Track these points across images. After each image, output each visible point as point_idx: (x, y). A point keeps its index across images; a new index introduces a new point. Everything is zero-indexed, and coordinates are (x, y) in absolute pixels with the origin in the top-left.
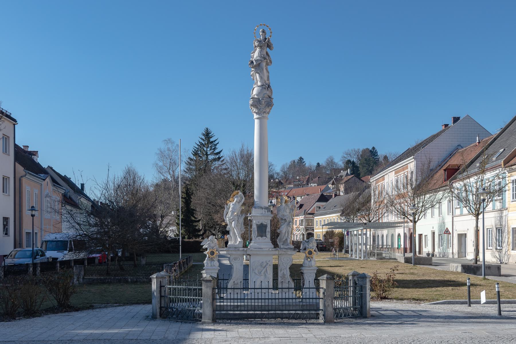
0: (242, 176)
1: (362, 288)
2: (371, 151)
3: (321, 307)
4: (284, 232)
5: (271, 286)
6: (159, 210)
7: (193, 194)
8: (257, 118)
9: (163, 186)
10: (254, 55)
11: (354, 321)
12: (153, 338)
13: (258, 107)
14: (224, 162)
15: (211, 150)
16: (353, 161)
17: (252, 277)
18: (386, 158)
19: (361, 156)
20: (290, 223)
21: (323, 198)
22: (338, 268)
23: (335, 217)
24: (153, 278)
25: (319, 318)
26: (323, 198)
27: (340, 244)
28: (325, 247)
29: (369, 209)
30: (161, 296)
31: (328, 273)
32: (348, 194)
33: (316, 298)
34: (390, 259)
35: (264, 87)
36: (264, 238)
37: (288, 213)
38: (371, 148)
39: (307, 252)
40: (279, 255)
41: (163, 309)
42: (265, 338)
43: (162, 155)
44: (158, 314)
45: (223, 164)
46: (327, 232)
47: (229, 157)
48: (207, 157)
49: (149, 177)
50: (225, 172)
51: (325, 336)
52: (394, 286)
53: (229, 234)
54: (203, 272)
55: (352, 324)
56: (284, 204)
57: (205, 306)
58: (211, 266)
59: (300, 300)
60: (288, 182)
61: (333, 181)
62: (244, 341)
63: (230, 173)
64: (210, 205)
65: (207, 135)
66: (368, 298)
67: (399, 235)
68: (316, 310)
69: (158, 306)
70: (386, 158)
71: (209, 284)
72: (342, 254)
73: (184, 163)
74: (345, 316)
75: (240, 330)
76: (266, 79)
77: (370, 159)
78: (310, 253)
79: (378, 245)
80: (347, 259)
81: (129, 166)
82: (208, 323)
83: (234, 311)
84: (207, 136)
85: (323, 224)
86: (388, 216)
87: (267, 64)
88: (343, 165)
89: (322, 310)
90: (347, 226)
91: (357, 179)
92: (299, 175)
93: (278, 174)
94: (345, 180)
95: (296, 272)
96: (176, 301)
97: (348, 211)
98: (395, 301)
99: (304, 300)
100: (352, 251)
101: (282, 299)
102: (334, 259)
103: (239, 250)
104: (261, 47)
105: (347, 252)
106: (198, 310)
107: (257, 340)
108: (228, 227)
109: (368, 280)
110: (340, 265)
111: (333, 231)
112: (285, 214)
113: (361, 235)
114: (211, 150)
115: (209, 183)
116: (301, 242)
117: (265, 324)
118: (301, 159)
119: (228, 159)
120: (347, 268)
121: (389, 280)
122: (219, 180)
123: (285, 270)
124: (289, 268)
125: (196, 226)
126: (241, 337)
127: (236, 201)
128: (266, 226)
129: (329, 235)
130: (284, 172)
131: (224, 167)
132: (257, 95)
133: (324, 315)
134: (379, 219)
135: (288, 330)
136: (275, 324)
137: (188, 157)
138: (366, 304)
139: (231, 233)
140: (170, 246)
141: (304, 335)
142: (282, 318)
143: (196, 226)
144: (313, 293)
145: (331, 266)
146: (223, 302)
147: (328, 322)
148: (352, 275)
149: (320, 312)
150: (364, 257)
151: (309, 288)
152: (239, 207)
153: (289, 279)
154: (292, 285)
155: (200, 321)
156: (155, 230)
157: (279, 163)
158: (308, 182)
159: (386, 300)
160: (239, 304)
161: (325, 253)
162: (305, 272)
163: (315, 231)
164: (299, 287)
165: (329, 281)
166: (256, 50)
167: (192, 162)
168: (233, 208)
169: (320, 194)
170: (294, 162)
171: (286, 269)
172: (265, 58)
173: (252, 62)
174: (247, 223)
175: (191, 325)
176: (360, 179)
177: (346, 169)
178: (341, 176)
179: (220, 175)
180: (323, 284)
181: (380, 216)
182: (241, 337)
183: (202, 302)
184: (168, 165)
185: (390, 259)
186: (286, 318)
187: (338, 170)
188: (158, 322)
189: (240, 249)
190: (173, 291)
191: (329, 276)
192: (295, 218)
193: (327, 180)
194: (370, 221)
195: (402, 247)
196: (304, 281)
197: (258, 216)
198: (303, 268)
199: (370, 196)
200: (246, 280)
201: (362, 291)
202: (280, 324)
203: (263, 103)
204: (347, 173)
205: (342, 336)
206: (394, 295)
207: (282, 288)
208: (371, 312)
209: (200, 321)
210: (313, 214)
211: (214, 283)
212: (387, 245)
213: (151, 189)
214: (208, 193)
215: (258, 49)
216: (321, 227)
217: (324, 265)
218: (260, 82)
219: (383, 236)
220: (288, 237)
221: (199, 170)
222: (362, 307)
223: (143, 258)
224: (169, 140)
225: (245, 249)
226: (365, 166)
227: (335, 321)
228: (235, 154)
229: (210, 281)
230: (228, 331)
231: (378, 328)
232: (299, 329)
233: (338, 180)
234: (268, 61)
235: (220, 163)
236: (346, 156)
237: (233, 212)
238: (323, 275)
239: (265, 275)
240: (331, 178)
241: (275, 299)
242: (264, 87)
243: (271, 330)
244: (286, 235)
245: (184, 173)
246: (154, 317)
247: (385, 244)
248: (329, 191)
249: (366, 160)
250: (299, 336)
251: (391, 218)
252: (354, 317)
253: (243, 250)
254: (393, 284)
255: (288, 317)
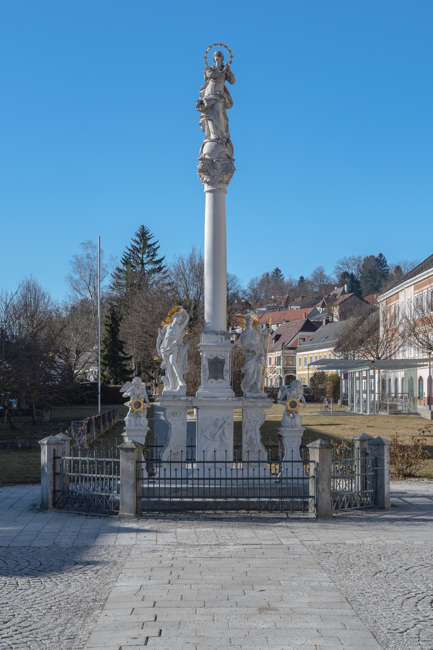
0: (192, 294)
1: (378, 462)
2: (377, 259)
3: (312, 492)
4: (251, 371)
5: (231, 458)
6: (73, 341)
7: (121, 319)
8: (210, 191)
9: (82, 310)
10: (204, 92)
11: (365, 514)
12: (36, 544)
13: (211, 173)
14: (167, 274)
15: (148, 256)
16: (352, 274)
17: (201, 443)
18: (398, 269)
19: (363, 266)
20: (261, 358)
21: (310, 326)
22: (333, 427)
23: (326, 353)
24: (43, 444)
25: (307, 510)
26: (310, 326)
27: (334, 392)
28: (313, 396)
29: (376, 341)
30: (55, 474)
31: (325, 437)
32: (345, 318)
33: (303, 478)
34: (409, 413)
35: (220, 141)
36: (220, 380)
37: (258, 342)
38: (376, 256)
39: (288, 403)
40: (244, 408)
41: (59, 494)
42: (219, 545)
43: (79, 264)
44: (51, 502)
45: (165, 278)
46: (315, 374)
47: (174, 266)
48: (143, 267)
49: (59, 296)
50: (169, 288)
51: (318, 543)
52: (424, 457)
53: (164, 374)
54: (125, 434)
55: (361, 520)
56: (251, 327)
57: (124, 489)
58: (136, 425)
59: (277, 480)
60: (258, 304)
61: (324, 302)
62: (184, 552)
63: (175, 290)
64: (145, 335)
65: (143, 235)
66: (387, 477)
67: (421, 379)
68: (303, 498)
69: (50, 489)
70: (398, 269)
71: (130, 454)
72: (338, 407)
73: (110, 276)
74: (349, 506)
75: (179, 530)
76: (223, 129)
77: (375, 271)
78: (294, 405)
79: (390, 393)
80: (345, 413)
81: (29, 277)
82: (129, 519)
83: (170, 497)
84: (143, 236)
85: (309, 362)
86: (404, 351)
87: (226, 107)
88: (337, 280)
89: (313, 497)
90: (344, 365)
91: (357, 299)
92: (273, 294)
93: (244, 292)
94: (340, 301)
95: (271, 433)
96: (78, 481)
97: (347, 343)
98: (426, 480)
99: (284, 481)
100: (352, 401)
101: (248, 479)
102: (326, 413)
103: (179, 400)
104: (215, 79)
105: (345, 403)
106: (115, 496)
107: (206, 549)
108: (163, 363)
109: (386, 448)
110: (335, 422)
111: (323, 373)
112: (253, 342)
113: (366, 378)
114: (148, 256)
115: (145, 303)
116: (278, 389)
117: (221, 519)
118: (277, 271)
119: (172, 269)
120: (347, 427)
121: (416, 447)
122: (159, 299)
123: (253, 432)
124: (261, 429)
125: (125, 365)
126: (180, 544)
127: (176, 323)
128: (222, 362)
129: (318, 378)
130: (253, 290)
131: (167, 281)
132: (209, 155)
133: (316, 506)
134: (391, 356)
135: (258, 531)
136: (237, 520)
137: (115, 267)
138: (383, 486)
139: (168, 373)
140: (83, 395)
141: (283, 541)
142: (248, 509)
143: (125, 365)
144: (297, 470)
145: (322, 425)
146: (154, 483)
147: (323, 517)
148: (360, 440)
149: (310, 500)
150: (372, 410)
151: (292, 462)
152: (181, 332)
153: (260, 446)
154: (265, 456)
155: (117, 514)
156: (69, 370)
157: (245, 274)
158: (287, 303)
159: (413, 479)
160: (179, 486)
161: (312, 405)
162: (284, 434)
163: (297, 373)
164: (275, 458)
165: (325, 450)
166: (207, 84)
167: (122, 275)
168: (171, 333)
169: (305, 319)
170: (268, 275)
171: (255, 430)
172: (221, 97)
173: (201, 103)
174: (194, 358)
175: (101, 520)
176: (362, 299)
177: (341, 285)
178: (335, 295)
179: (161, 292)
180: (315, 455)
181: (393, 352)
182: (180, 544)
183: (119, 482)
184: (87, 279)
185: (409, 413)
186: (255, 509)
187: (331, 287)
188: (50, 515)
189: (183, 398)
190: (74, 465)
191: (324, 442)
192: (269, 355)
193: (314, 300)
194: (379, 358)
195: (426, 395)
196: (283, 449)
197: (209, 346)
198: (282, 429)
199: (378, 321)
200: (192, 446)
201: (377, 466)
202: (245, 519)
203: (219, 166)
204: (344, 290)
205: (348, 542)
206: (423, 471)
207: (248, 462)
208: (392, 499)
209: (117, 514)
210: (294, 349)
211: (139, 452)
212: (402, 393)
213: (64, 314)
214: (143, 318)
215: (211, 83)
216: (306, 367)
217: (313, 422)
218: (214, 134)
219: (396, 380)
220: (258, 378)
221: (131, 286)
222: (376, 492)
223: (46, 411)
224: (89, 243)
225: (190, 398)
226: (369, 281)
227: (334, 515)
228: (183, 263)
229: (132, 450)
230: (160, 532)
231: (405, 528)
232: (276, 529)
233: (329, 302)
234: (227, 101)
235: (161, 275)
236: (341, 266)
237: (170, 340)
238: (314, 439)
239: (222, 440)
240: (319, 299)
241: (237, 479)
242: (220, 141)
243: (230, 530)
244: (255, 377)
245: (110, 291)
246: (41, 507)
247: (400, 391)
248: (317, 316)
249: (370, 272)
250: (275, 542)
251: (411, 353)
252: (364, 507)
253: (187, 400)
254: (422, 454)
255: (259, 507)
